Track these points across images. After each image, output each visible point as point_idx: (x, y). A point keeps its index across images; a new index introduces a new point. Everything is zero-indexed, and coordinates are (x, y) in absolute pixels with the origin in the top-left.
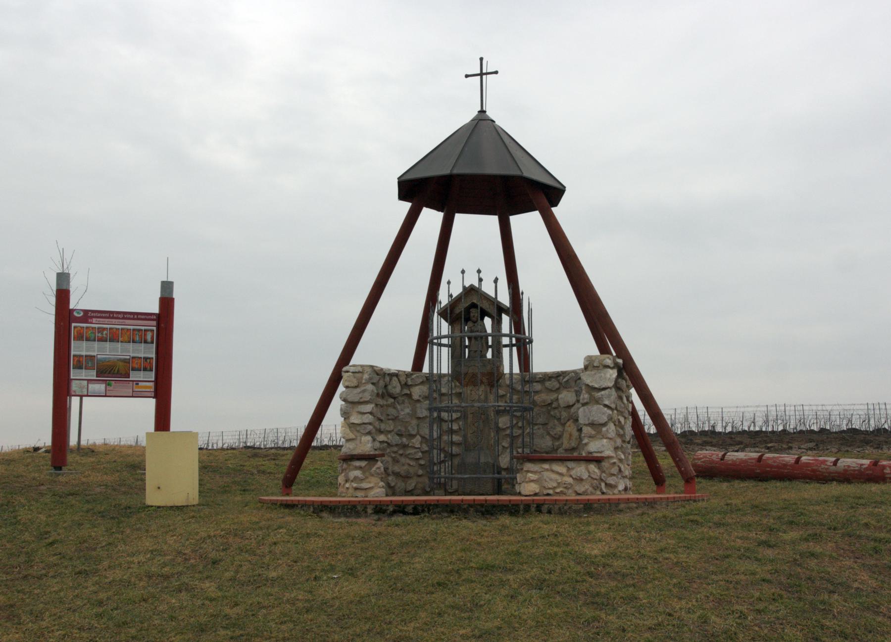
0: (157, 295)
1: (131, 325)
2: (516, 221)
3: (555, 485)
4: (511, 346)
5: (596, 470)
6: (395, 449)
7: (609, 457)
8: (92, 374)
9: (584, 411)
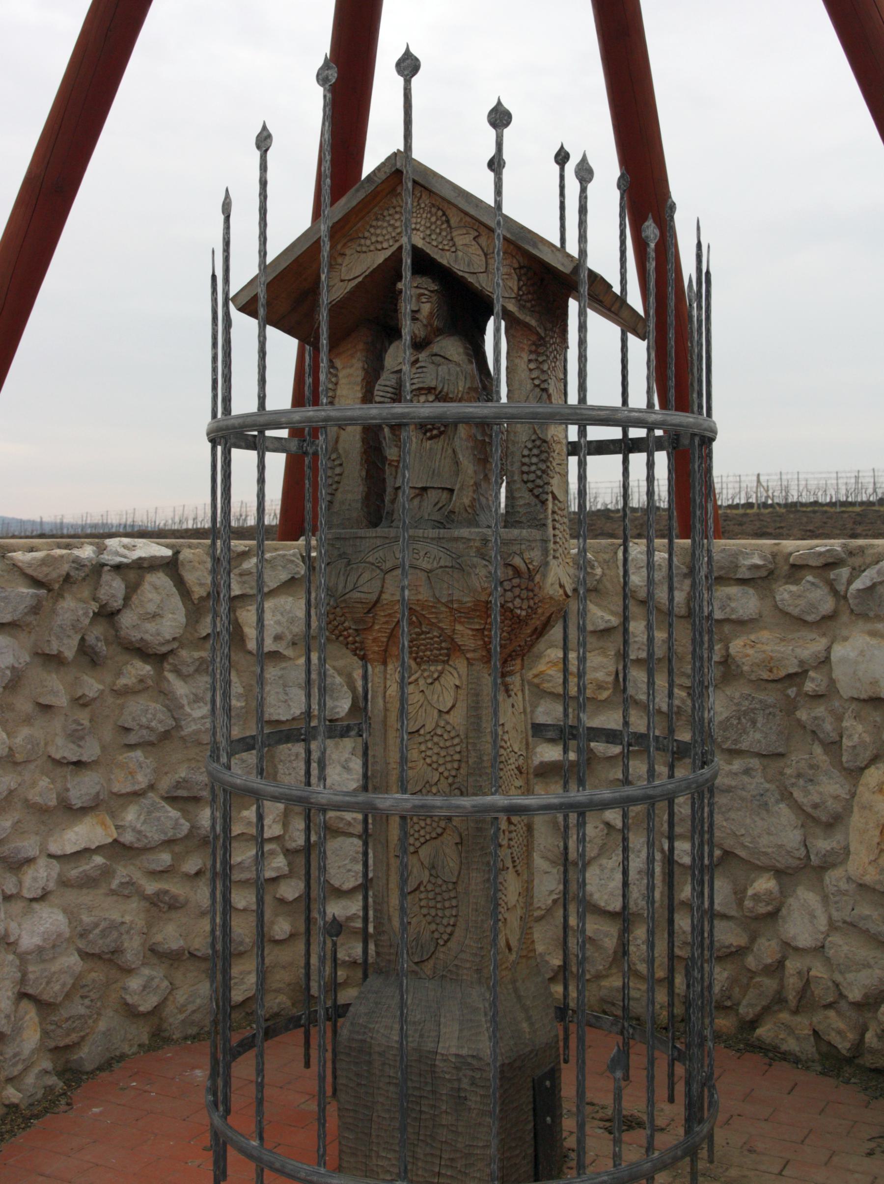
2: (632, 456)
6: (165, 858)
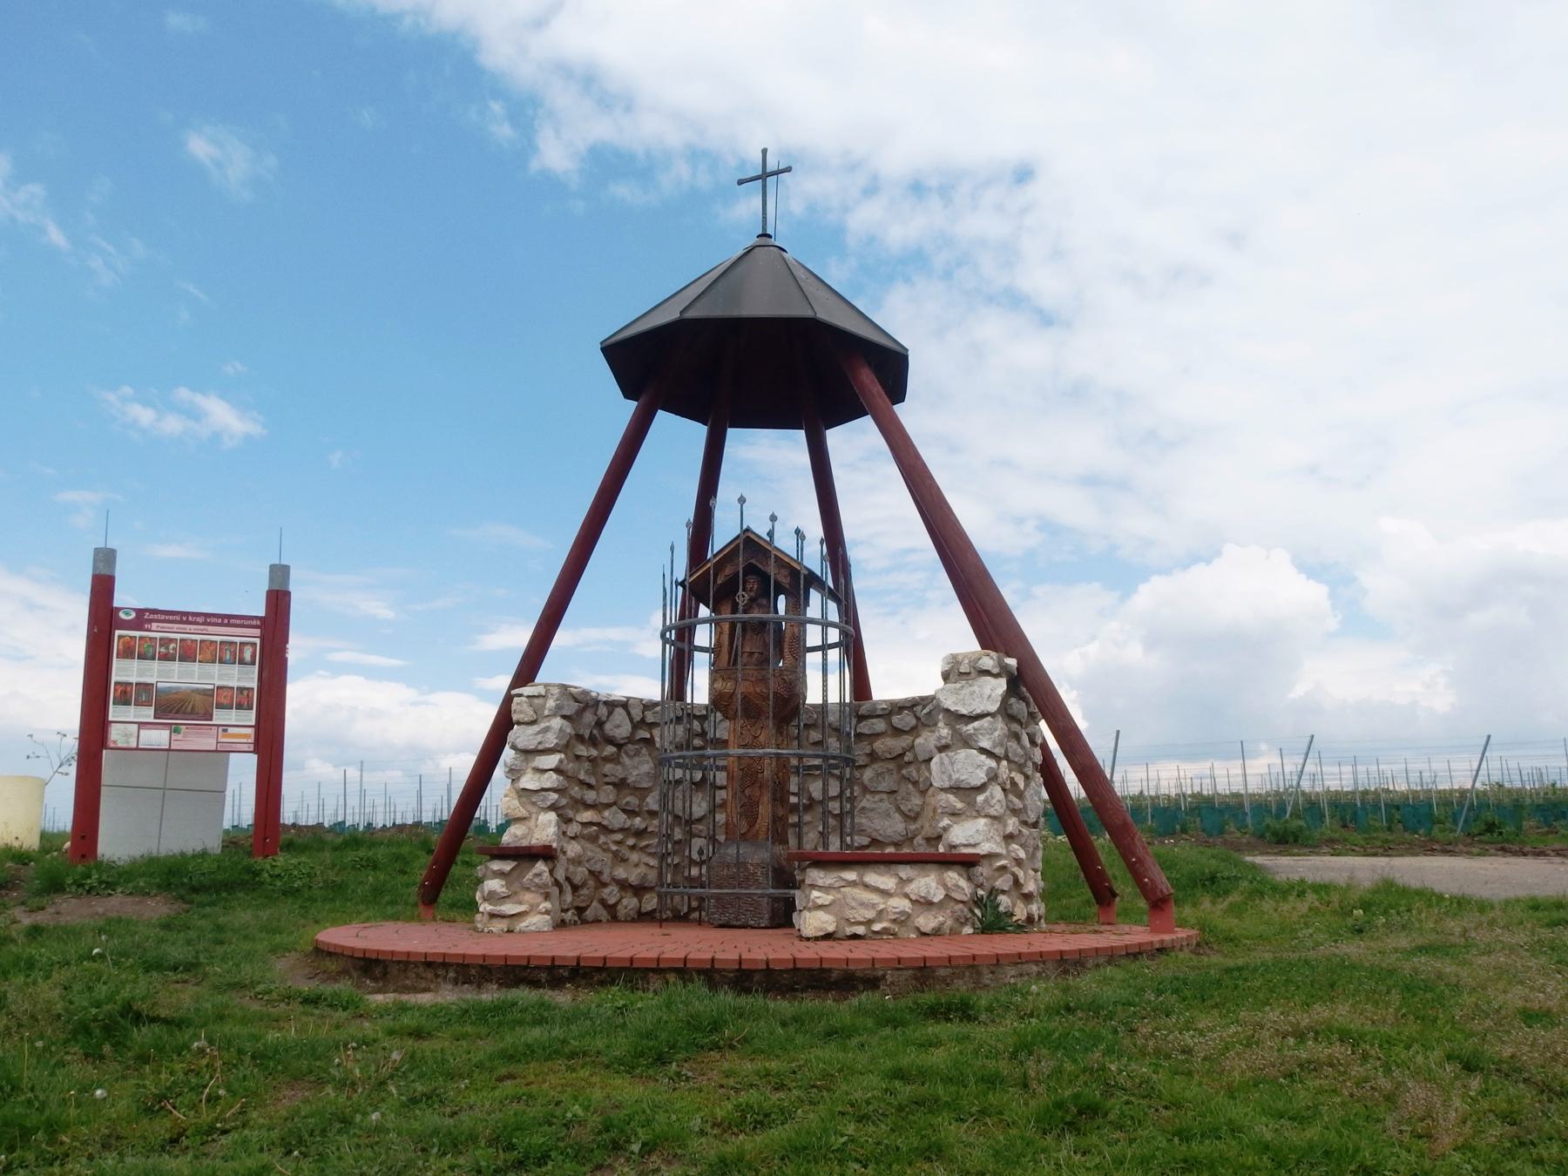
0: (264, 587)
1: (218, 634)
3: (870, 914)
4: (824, 648)
5: (963, 883)
6: (619, 837)
7: (991, 856)
8: (148, 714)
9: (942, 763)
